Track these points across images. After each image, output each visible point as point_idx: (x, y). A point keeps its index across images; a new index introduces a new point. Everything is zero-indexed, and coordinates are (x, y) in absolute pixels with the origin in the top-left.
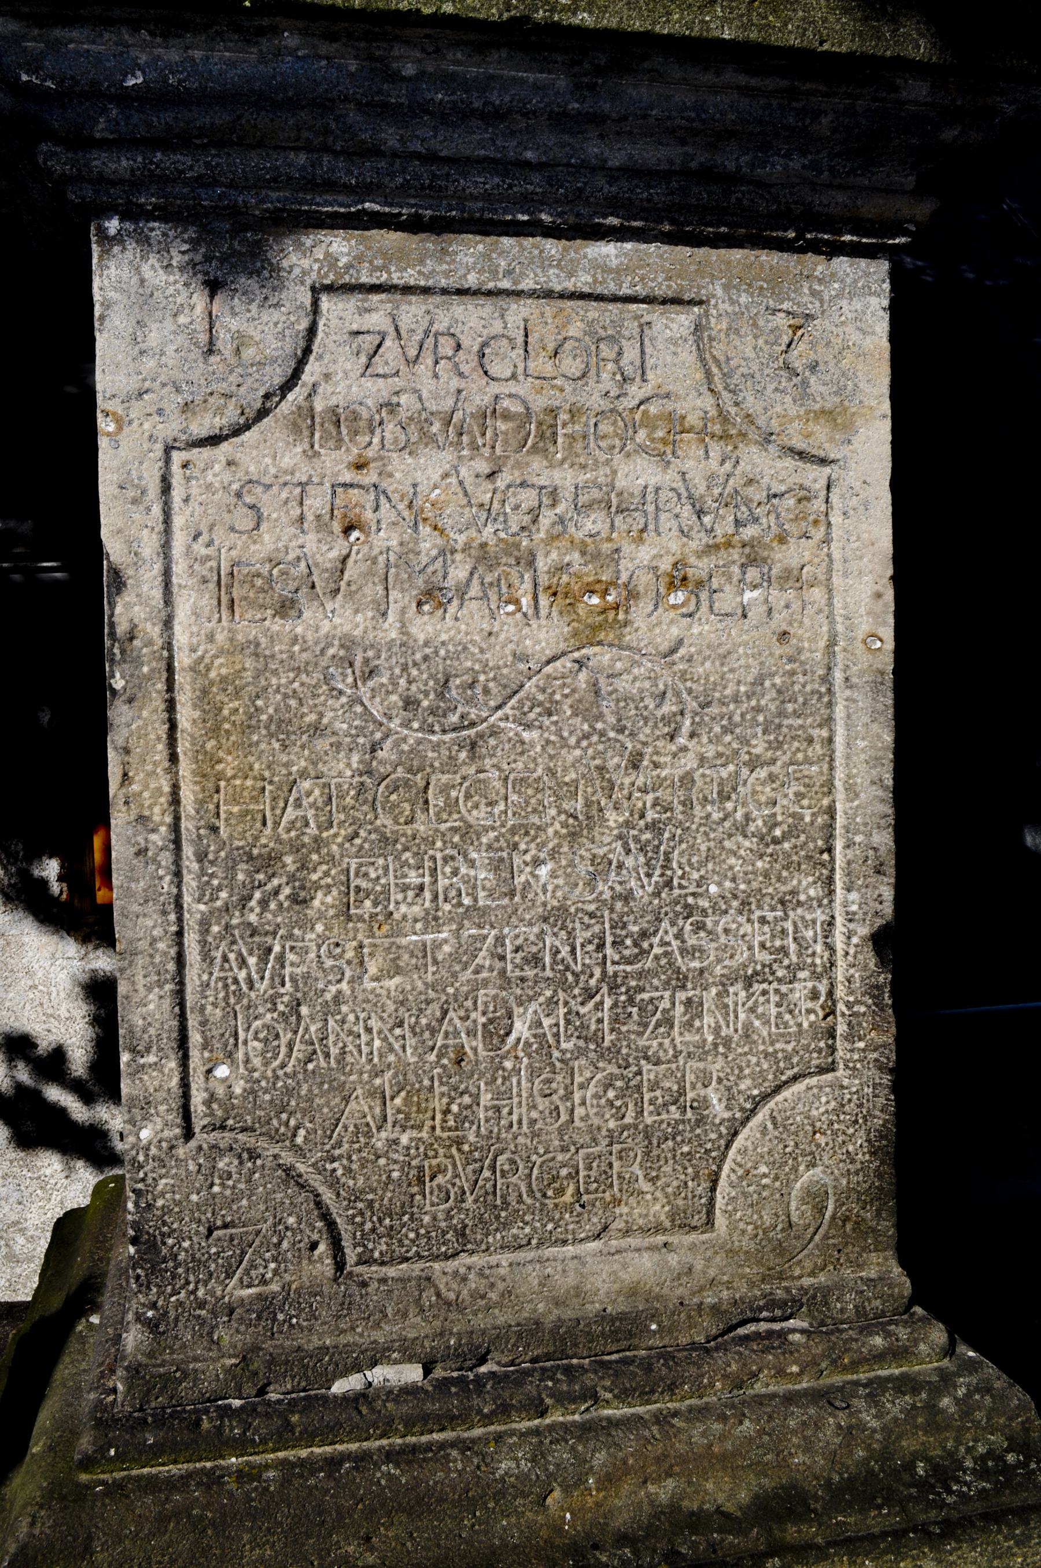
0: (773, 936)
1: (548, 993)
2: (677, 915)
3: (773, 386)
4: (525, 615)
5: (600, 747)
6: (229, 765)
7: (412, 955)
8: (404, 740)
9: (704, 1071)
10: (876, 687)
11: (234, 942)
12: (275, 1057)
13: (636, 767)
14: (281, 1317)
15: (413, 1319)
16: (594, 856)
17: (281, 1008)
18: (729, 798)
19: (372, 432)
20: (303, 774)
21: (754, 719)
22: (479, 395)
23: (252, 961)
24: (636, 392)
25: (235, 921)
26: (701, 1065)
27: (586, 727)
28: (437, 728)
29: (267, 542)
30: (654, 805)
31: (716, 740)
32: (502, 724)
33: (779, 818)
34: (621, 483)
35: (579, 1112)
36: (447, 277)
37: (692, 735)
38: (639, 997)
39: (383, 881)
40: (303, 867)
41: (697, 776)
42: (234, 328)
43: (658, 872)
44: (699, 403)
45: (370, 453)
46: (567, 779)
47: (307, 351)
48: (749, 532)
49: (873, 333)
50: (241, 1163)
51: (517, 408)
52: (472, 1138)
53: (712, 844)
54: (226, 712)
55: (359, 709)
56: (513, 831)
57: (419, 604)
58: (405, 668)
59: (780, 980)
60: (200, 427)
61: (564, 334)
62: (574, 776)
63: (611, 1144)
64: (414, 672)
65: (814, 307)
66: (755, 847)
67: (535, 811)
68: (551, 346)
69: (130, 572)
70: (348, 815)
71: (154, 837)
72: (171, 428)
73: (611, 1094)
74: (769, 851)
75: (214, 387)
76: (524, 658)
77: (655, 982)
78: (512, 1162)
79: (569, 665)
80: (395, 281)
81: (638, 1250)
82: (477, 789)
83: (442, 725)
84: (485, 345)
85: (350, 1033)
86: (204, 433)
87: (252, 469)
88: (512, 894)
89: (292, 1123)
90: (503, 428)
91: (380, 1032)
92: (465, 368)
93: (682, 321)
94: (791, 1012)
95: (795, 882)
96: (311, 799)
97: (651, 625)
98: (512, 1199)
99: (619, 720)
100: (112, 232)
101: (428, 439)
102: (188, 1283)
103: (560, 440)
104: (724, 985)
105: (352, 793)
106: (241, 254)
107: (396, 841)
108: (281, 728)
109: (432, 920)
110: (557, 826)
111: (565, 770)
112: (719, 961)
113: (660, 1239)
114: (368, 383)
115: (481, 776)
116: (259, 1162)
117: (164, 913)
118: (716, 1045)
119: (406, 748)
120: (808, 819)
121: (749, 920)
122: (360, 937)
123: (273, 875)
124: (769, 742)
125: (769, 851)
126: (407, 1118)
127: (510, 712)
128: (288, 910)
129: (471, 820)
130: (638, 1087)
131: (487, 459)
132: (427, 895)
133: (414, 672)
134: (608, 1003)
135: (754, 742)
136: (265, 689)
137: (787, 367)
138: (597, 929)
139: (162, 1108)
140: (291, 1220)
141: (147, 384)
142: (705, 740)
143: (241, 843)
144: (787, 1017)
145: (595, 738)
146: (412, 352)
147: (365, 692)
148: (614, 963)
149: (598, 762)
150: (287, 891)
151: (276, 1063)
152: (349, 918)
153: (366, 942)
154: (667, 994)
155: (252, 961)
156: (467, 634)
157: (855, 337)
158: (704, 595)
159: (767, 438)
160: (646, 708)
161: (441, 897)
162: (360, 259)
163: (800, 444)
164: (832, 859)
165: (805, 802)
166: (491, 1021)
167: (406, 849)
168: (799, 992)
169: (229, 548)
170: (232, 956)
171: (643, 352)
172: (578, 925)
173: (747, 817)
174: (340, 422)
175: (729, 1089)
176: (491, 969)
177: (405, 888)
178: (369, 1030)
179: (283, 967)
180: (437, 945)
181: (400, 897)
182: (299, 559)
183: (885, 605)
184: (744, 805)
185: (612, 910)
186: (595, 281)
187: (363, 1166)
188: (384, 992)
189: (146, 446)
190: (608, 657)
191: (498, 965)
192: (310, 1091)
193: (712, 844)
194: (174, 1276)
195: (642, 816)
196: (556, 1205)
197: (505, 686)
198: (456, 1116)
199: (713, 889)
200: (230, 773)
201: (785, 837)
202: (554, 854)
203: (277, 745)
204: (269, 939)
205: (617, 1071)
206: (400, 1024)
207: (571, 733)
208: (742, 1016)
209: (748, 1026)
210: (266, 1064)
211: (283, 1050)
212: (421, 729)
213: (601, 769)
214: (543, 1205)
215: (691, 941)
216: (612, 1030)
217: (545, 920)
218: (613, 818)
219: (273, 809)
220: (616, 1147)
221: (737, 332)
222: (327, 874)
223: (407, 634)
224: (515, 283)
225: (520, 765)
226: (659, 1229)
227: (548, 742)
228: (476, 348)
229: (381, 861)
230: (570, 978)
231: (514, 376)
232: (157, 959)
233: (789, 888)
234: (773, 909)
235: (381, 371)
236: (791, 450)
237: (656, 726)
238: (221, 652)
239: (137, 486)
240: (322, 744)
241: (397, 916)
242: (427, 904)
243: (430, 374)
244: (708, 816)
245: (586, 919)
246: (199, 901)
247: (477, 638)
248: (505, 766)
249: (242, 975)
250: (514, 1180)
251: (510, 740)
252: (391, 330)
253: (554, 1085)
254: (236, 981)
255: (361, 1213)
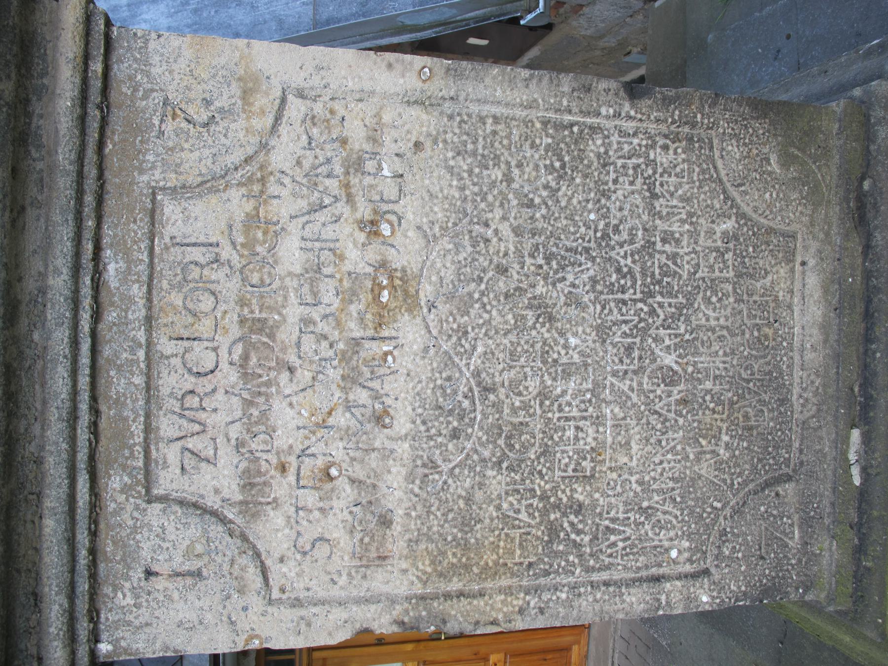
0: (626, 175)
1: (650, 340)
2: (608, 245)
3: (223, 139)
4: (395, 348)
5: (492, 295)
6: (490, 558)
7: (619, 434)
8: (479, 439)
9: (707, 232)
10: (458, 75)
11: (601, 551)
12: (670, 522)
13: (506, 270)
14: (812, 513)
15: (823, 433)
16: (565, 304)
17: (642, 519)
18: (532, 200)
19: (258, 459)
20: (498, 508)
21: (477, 176)
22: (229, 376)
23: (613, 538)
24: (227, 252)
25: (588, 550)
26: (702, 234)
27: (477, 306)
28: (472, 416)
29: (338, 534)
30: (534, 257)
31: (491, 205)
32: (472, 368)
33: (548, 162)
34: (298, 269)
35: (722, 321)
36: (137, 400)
37: (487, 225)
38: (657, 277)
39: (571, 454)
40: (558, 507)
41: (515, 224)
42: (181, 559)
43: (579, 256)
44: (235, 202)
45: (274, 461)
46: (512, 322)
47: (195, 505)
48: (338, 170)
49: (180, 48)
50: (728, 541)
51: (239, 349)
52: (730, 395)
53: (563, 215)
54: (455, 560)
55: (457, 471)
56: (544, 362)
57: (384, 427)
58: (430, 438)
59: (655, 173)
60: (253, 575)
61: (180, 309)
62: (510, 316)
63: (743, 301)
64: (433, 431)
65: (157, 97)
66: (567, 183)
67: (532, 346)
68: (190, 320)
69: (358, 626)
70: (527, 478)
71: (532, 604)
72: (256, 603)
73: (714, 299)
74: (570, 172)
75: (226, 573)
76: (426, 349)
77: (649, 264)
78: (746, 369)
79: (432, 316)
80: (141, 439)
81: (804, 285)
82: (514, 387)
83: (471, 412)
84: (190, 371)
85: (662, 474)
86: (260, 579)
87: (286, 546)
88: (586, 365)
89: (709, 510)
90: (255, 360)
91: (663, 455)
92: (209, 388)
93: (170, 209)
94: (675, 166)
95: (592, 155)
96: (515, 502)
97: (406, 251)
98: (767, 368)
99: (474, 280)
100: (110, 647)
101: (264, 415)
102: (787, 570)
103: (264, 315)
104: (655, 215)
105: (513, 474)
106: (124, 553)
107: (546, 445)
108: (467, 523)
109: (598, 421)
110: (544, 330)
111: (506, 322)
112: (639, 216)
113: (798, 267)
114: (221, 463)
115: (506, 384)
116: (728, 530)
117: (580, 595)
118: (692, 223)
119: (485, 438)
120: (550, 141)
121: (615, 192)
122: (604, 469)
123: (562, 526)
124: (494, 165)
125: (570, 172)
126: (714, 437)
127: (464, 362)
128: (584, 516)
129: (535, 393)
130: (712, 280)
131: (279, 374)
132: (581, 424)
133: (433, 431)
134: (659, 298)
135: (493, 177)
136: (441, 535)
137: (206, 125)
138: (612, 304)
139: (692, 590)
140: (762, 509)
141: (225, 619)
142: (490, 215)
143: (540, 548)
144: (678, 170)
145: (485, 300)
146: (197, 428)
147: (445, 467)
148: (635, 293)
149: (502, 298)
150: (572, 517)
151: (674, 521)
152: (593, 476)
153: (608, 464)
154: (657, 256)
155: (613, 538)
156: (408, 392)
157: (182, 64)
158: (385, 207)
159: (264, 147)
160: (465, 259)
161: (585, 414)
162: (124, 467)
163: (269, 120)
164: (577, 123)
165: (538, 141)
166: (664, 381)
167: (552, 438)
168: (663, 159)
169: (343, 560)
170: (609, 551)
171: (194, 245)
172: (609, 318)
173: (546, 187)
174: (252, 482)
175: (719, 216)
176: (632, 380)
177: (577, 439)
178: (661, 462)
179: (618, 519)
180: (614, 417)
181: (582, 442)
182: (351, 512)
183: (397, 61)
184: (537, 189)
185: (602, 293)
186: (138, 281)
187: (739, 466)
188: (640, 453)
189: (269, 617)
190: (428, 287)
191: (630, 375)
192: (692, 500)
193: (563, 215)
194: (784, 578)
195: (541, 267)
196: (774, 340)
197: (446, 365)
198: (717, 405)
199: (592, 216)
200: (495, 557)
201: (561, 159)
202: (562, 334)
203: (479, 526)
204: (601, 528)
205: (701, 295)
206: (660, 441)
207: (481, 317)
208: (675, 202)
209: (682, 199)
210: (674, 527)
211: (667, 516)
212: (472, 427)
213: (507, 296)
214: (773, 348)
215: (625, 236)
216: (677, 297)
217: (604, 341)
218: (540, 289)
219: (520, 528)
220: (745, 297)
221: (178, 165)
222: (564, 492)
223: (406, 435)
224: (140, 346)
225: (501, 356)
226: (792, 270)
227: (486, 334)
228: (193, 379)
229: (558, 455)
230: (642, 324)
231: (215, 349)
232: (607, 597)
233: (595, 160)
234: (608, 173)
235: (212, 452)
236: (274, 127)
237: (479, 253)
238: (414, 565)
239: (298, 624)
240: (479, 495)
241: (594, 444)
242: (588, 423)
243: (213, 415)
244: (544, 217)
245: (606, 311)
246: (573, 573)
247: (411, 385)
248: (501, 366)
249: (621, 544)
250: (756, 367)
251: (483, 363)
252: (179, 444)
253: (705, 338)
254: (624, 549)
255: (764, 466)
